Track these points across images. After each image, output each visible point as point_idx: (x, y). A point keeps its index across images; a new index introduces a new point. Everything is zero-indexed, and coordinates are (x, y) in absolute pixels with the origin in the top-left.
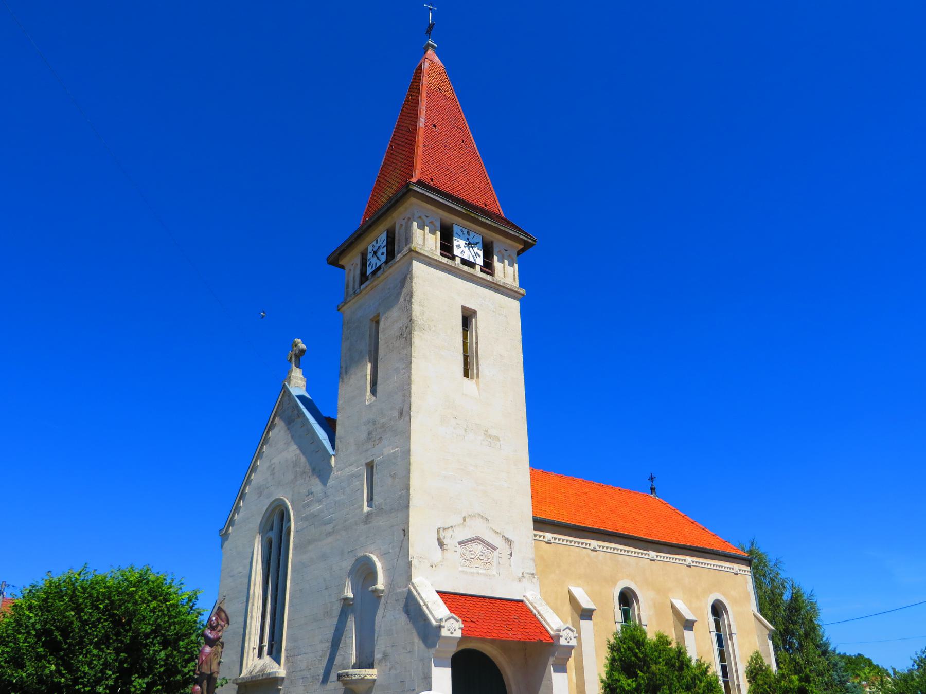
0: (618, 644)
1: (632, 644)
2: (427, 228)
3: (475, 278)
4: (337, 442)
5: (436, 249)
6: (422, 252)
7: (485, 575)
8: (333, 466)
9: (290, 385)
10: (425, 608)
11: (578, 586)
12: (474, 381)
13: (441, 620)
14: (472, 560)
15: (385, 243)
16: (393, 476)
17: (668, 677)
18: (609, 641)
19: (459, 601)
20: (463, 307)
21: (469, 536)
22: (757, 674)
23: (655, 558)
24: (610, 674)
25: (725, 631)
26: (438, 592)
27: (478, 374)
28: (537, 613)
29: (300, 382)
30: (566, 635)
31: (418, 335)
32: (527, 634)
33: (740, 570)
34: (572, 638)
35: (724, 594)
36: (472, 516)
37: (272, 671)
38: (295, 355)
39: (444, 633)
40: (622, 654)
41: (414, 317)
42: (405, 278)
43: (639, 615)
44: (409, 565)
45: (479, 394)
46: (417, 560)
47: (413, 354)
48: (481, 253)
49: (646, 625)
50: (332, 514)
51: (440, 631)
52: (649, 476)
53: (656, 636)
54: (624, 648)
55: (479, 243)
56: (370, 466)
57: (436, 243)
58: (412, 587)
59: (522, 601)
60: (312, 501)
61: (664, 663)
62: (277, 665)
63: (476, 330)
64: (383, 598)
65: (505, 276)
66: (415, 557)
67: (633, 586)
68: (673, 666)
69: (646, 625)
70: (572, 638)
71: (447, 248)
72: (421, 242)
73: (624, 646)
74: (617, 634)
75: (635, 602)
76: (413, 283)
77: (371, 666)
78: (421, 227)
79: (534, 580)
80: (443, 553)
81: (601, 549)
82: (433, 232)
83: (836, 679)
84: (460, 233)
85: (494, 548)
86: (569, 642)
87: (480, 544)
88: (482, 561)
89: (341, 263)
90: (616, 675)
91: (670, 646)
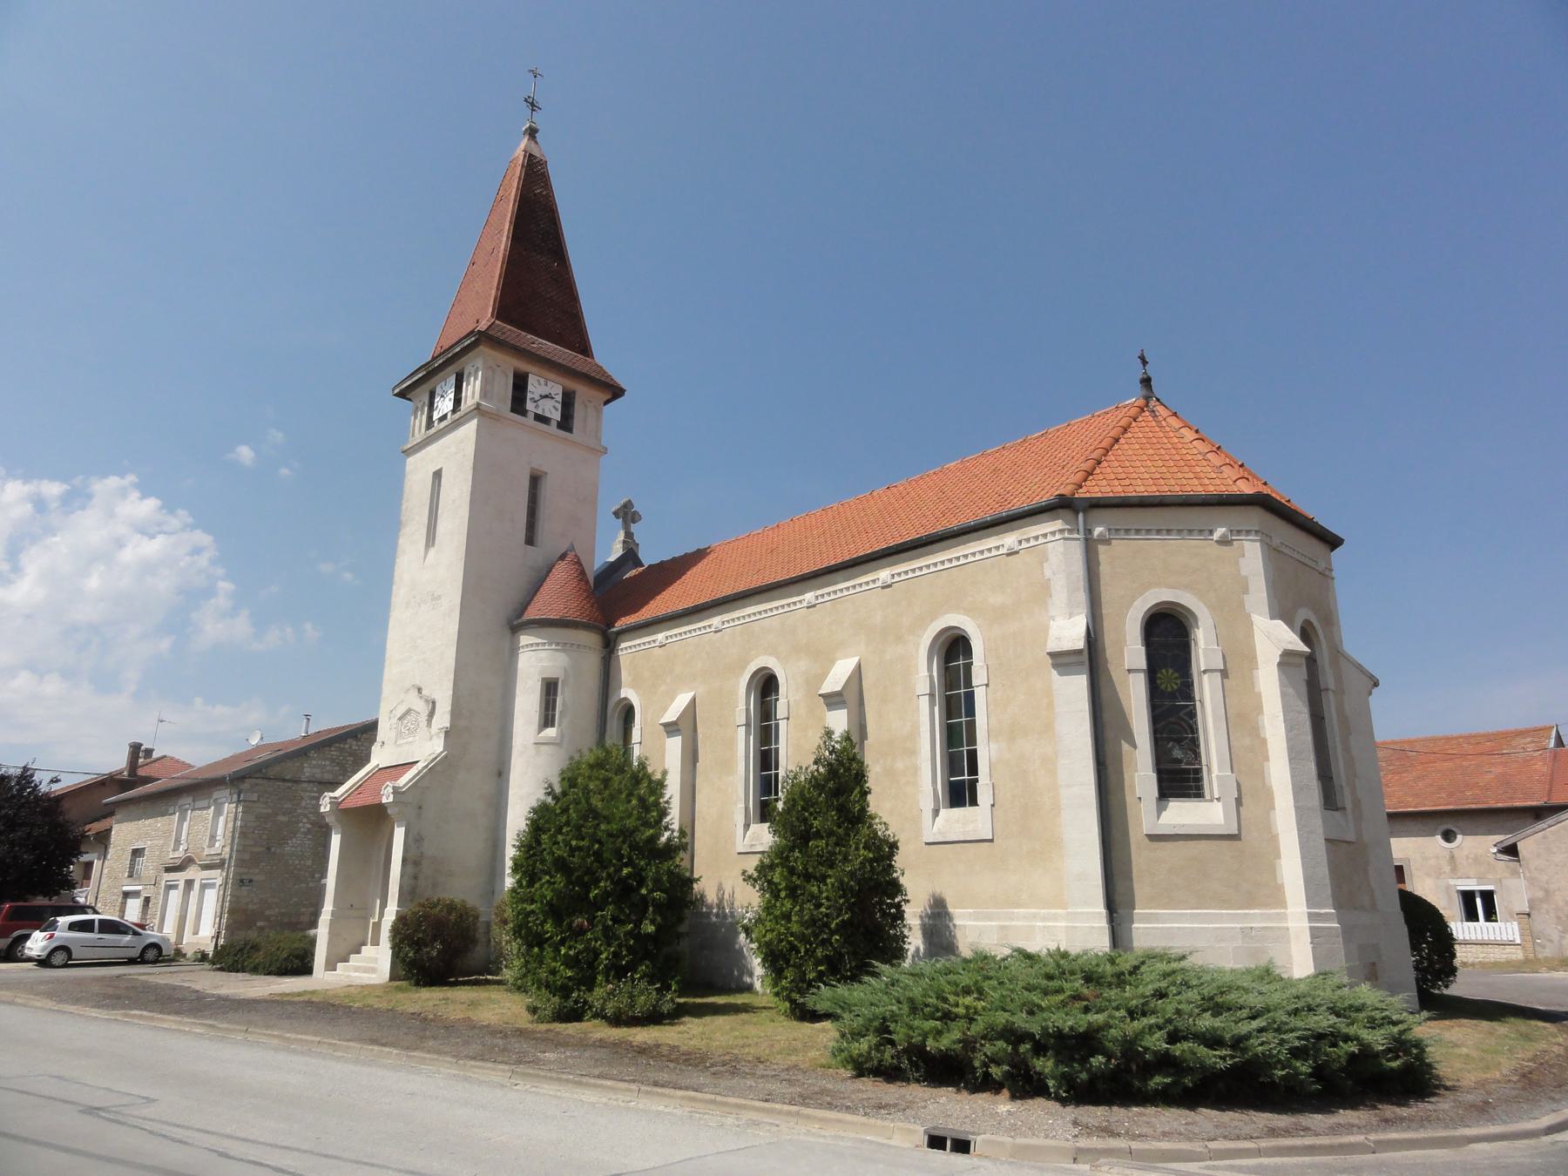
84: (536, 384)
89: (408, 397)
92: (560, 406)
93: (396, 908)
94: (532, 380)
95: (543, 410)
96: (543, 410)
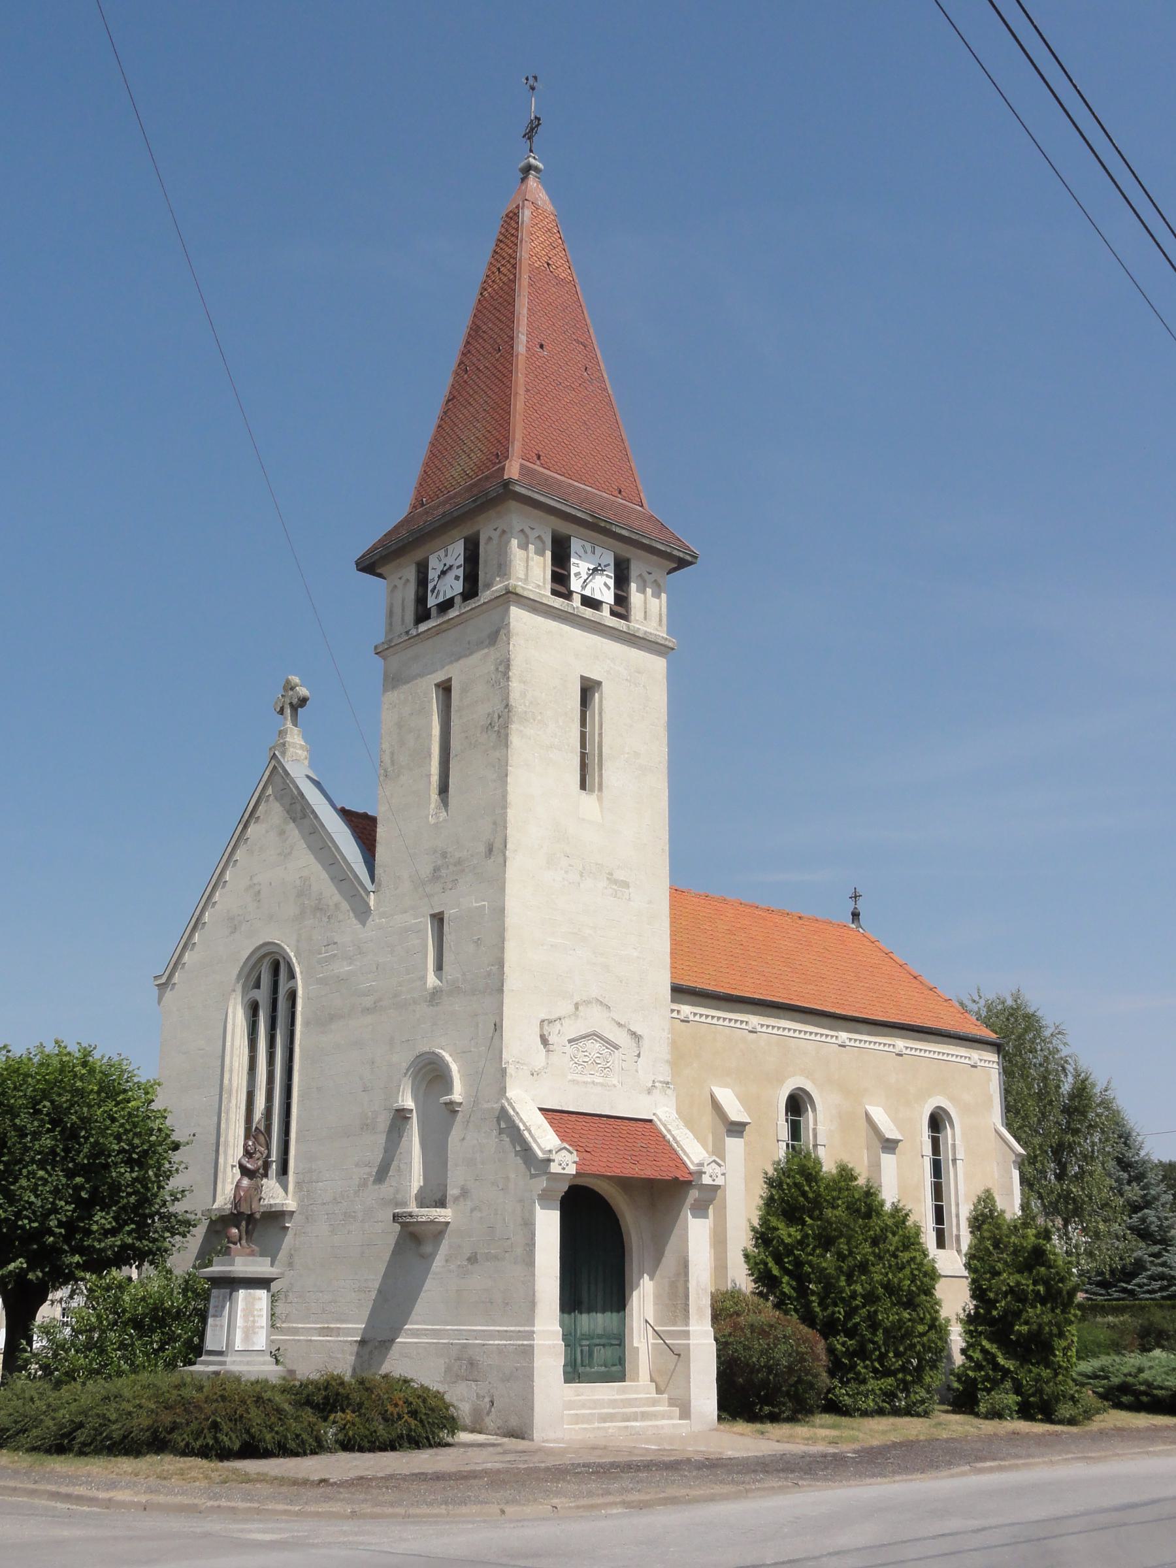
0: (780, 1178)
1: (799, 1179)
2: (531, 547)
3: (603, 627)
4: (378, 871)
5: (544, 584)
6: (525, 594)
7: (602, 1085)
8: (372, 908)
9: (284, 758)
10: (526, 1134)
11: (726, 1086)
12: (595, 796)
13: (550, 1151)
14: (585, 1064)
15: (461, 561)
16: (478, 942)
17: (847, 1226)
18: (766, 1173)
19: (568, 1122)
20: (582, 677)
21: (583, 1032)
22: (984, 1222)
23: (848, 1043)
24: (764, 1221)
25: (946, 1155)
26: (541, 1109)
27: (600, 785)
28: (671, 1139)
29: (300, 752)
30: (711, 1171)
31: (517, 729)
32: (658, 1169)
33: (981, 1060)
34: (719, 1175)
35: (952, 1099)
36: (587, 1003)
37: (272, 1202)
38: (291, 704)
39: (554, 1168)
40: (784, 1193)
41: (512, 702)
42: (497, 632)
43: (814, 1129)
44: (503, 1072)
45: (602, 817)
46: (513, 1066)
47: (510, 761)
48: (611, 583)
49: (824, 1146)
50: (373, 981)
51: (549, 1166)
52: (851, 893)
53: (837, 1168)
54: (788, 1184)
55: (609, 565)
56: (438, 919)
57: (544, 573)
58: (506, 1104)
59: (650, 1121)
60: (335, 955)
61: (844, 1206)
62: (281, 1191)
63: (600, 714)
64: (460, 1114)
65: (645, 618)
66: (510, 1061)
67: (809, 1087)
68: (858, 1210)
69: (824, 1146)
70: (719, 1175)
71: (560, 579)
72: (521, 575)
73: (788, 1180)
74: (778, 1163)
75: (809, 1109)
76: (511, 645)
77: (441, 1203)
78: (524, 546)
79: (669, 1092)
80: (547, 1057)
81: (764, 1029)
82: (540, 553)
83: (1154, 1222)
84: (581, 552)
85: (617, 1047)
86: (714, 1180)
87: (596, 1041)
88: (599, 1066)
89: (379, 571)
90: (774, 1222)
91: (856, 1183)
92: (612, 581)
93: (691, 1328)
94: (576, 545)
95: (593, 589)
96: (593, 589)
